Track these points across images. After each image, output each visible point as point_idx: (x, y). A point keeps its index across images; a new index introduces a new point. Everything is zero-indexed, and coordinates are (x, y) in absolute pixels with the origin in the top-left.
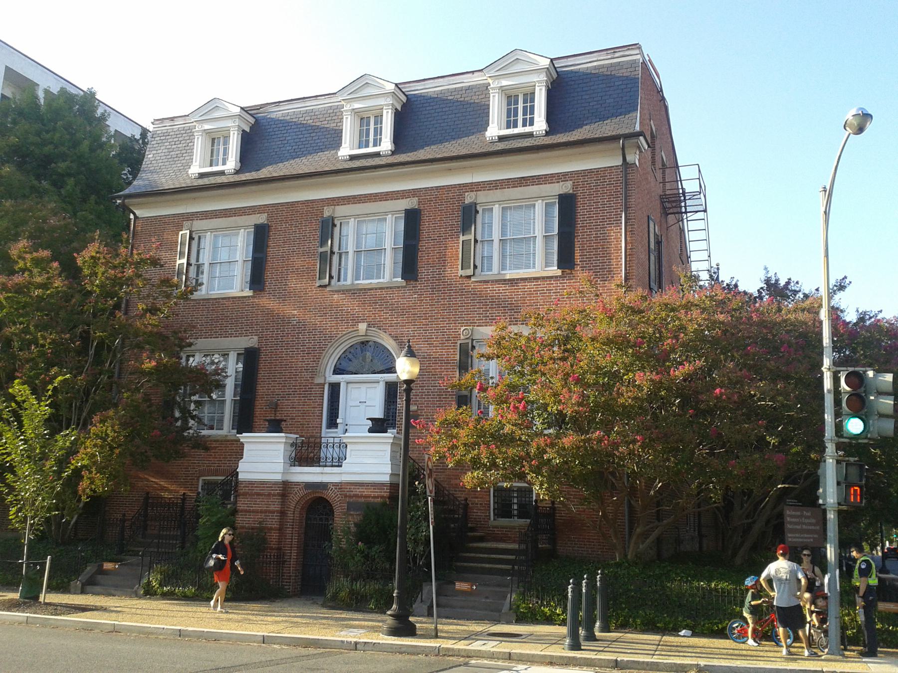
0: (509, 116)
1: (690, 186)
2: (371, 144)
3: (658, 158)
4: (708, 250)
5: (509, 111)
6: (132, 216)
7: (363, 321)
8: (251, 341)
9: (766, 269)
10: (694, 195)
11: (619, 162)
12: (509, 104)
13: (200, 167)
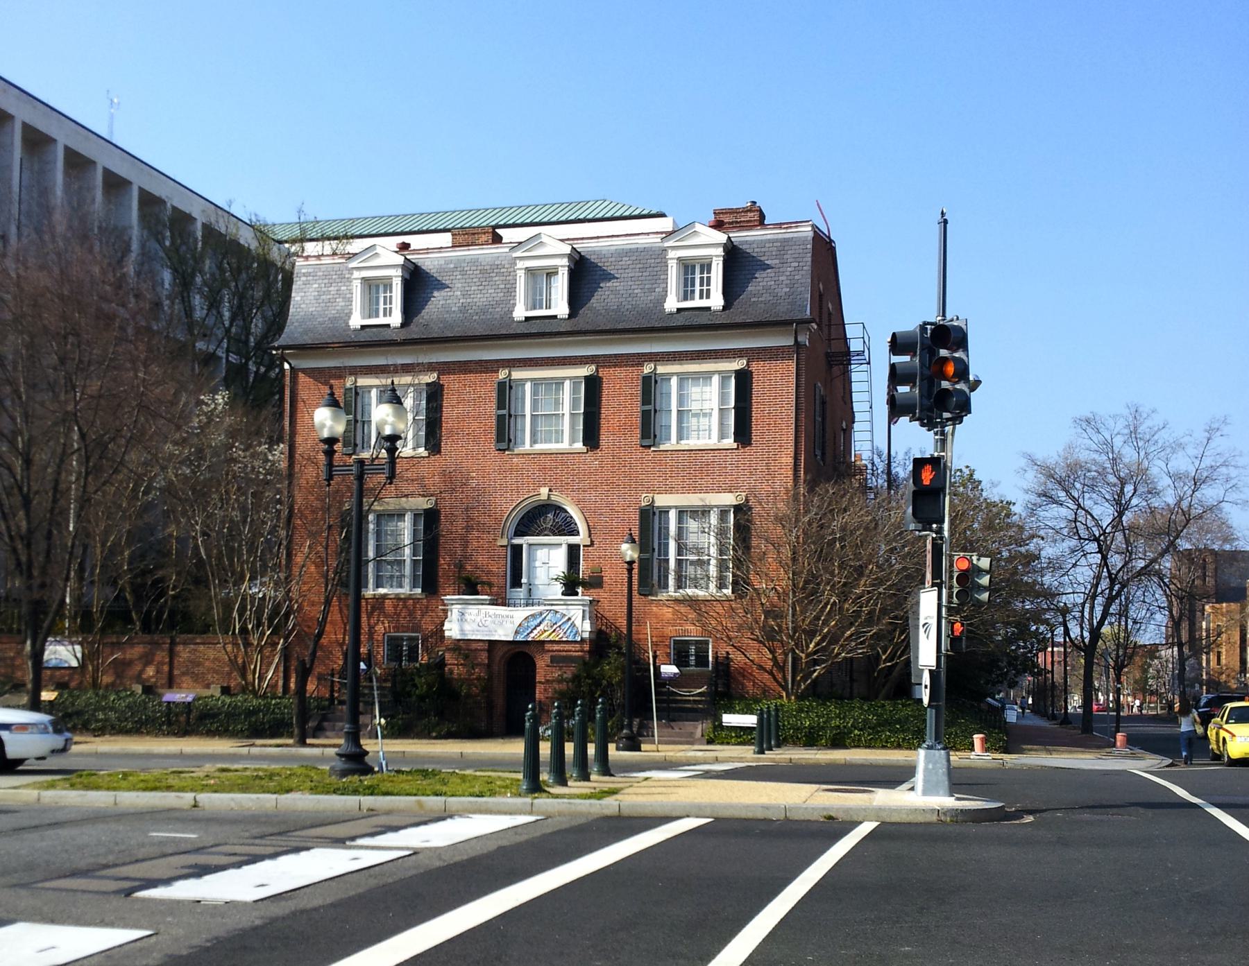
0: (686, 285)
1: (855, 346)
2: (571, 772)
3: (825, 310)
4: (871, 421)
5: (686, 280)
6: (286, 366)
7: (545, 485)
8: (424, 503)
9: (943, 213)
10: (861, 353)
11: (791, 342)
12: (686, 273)
13: (363, 318)
